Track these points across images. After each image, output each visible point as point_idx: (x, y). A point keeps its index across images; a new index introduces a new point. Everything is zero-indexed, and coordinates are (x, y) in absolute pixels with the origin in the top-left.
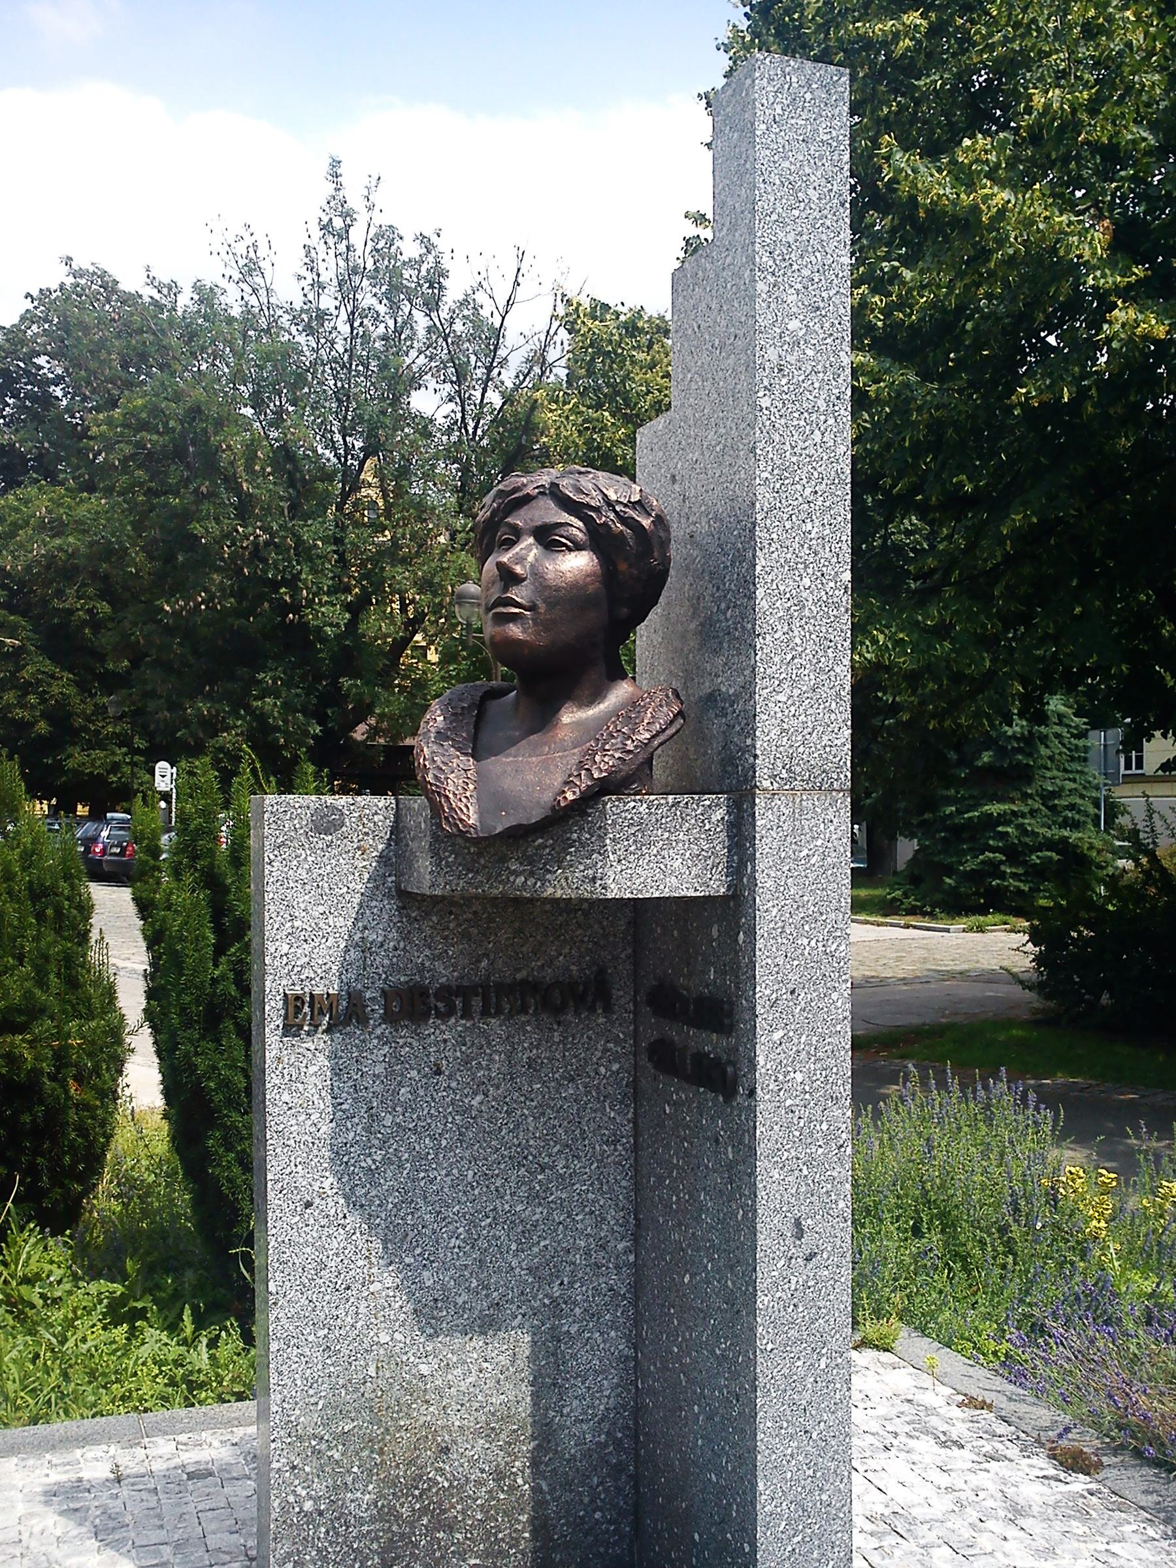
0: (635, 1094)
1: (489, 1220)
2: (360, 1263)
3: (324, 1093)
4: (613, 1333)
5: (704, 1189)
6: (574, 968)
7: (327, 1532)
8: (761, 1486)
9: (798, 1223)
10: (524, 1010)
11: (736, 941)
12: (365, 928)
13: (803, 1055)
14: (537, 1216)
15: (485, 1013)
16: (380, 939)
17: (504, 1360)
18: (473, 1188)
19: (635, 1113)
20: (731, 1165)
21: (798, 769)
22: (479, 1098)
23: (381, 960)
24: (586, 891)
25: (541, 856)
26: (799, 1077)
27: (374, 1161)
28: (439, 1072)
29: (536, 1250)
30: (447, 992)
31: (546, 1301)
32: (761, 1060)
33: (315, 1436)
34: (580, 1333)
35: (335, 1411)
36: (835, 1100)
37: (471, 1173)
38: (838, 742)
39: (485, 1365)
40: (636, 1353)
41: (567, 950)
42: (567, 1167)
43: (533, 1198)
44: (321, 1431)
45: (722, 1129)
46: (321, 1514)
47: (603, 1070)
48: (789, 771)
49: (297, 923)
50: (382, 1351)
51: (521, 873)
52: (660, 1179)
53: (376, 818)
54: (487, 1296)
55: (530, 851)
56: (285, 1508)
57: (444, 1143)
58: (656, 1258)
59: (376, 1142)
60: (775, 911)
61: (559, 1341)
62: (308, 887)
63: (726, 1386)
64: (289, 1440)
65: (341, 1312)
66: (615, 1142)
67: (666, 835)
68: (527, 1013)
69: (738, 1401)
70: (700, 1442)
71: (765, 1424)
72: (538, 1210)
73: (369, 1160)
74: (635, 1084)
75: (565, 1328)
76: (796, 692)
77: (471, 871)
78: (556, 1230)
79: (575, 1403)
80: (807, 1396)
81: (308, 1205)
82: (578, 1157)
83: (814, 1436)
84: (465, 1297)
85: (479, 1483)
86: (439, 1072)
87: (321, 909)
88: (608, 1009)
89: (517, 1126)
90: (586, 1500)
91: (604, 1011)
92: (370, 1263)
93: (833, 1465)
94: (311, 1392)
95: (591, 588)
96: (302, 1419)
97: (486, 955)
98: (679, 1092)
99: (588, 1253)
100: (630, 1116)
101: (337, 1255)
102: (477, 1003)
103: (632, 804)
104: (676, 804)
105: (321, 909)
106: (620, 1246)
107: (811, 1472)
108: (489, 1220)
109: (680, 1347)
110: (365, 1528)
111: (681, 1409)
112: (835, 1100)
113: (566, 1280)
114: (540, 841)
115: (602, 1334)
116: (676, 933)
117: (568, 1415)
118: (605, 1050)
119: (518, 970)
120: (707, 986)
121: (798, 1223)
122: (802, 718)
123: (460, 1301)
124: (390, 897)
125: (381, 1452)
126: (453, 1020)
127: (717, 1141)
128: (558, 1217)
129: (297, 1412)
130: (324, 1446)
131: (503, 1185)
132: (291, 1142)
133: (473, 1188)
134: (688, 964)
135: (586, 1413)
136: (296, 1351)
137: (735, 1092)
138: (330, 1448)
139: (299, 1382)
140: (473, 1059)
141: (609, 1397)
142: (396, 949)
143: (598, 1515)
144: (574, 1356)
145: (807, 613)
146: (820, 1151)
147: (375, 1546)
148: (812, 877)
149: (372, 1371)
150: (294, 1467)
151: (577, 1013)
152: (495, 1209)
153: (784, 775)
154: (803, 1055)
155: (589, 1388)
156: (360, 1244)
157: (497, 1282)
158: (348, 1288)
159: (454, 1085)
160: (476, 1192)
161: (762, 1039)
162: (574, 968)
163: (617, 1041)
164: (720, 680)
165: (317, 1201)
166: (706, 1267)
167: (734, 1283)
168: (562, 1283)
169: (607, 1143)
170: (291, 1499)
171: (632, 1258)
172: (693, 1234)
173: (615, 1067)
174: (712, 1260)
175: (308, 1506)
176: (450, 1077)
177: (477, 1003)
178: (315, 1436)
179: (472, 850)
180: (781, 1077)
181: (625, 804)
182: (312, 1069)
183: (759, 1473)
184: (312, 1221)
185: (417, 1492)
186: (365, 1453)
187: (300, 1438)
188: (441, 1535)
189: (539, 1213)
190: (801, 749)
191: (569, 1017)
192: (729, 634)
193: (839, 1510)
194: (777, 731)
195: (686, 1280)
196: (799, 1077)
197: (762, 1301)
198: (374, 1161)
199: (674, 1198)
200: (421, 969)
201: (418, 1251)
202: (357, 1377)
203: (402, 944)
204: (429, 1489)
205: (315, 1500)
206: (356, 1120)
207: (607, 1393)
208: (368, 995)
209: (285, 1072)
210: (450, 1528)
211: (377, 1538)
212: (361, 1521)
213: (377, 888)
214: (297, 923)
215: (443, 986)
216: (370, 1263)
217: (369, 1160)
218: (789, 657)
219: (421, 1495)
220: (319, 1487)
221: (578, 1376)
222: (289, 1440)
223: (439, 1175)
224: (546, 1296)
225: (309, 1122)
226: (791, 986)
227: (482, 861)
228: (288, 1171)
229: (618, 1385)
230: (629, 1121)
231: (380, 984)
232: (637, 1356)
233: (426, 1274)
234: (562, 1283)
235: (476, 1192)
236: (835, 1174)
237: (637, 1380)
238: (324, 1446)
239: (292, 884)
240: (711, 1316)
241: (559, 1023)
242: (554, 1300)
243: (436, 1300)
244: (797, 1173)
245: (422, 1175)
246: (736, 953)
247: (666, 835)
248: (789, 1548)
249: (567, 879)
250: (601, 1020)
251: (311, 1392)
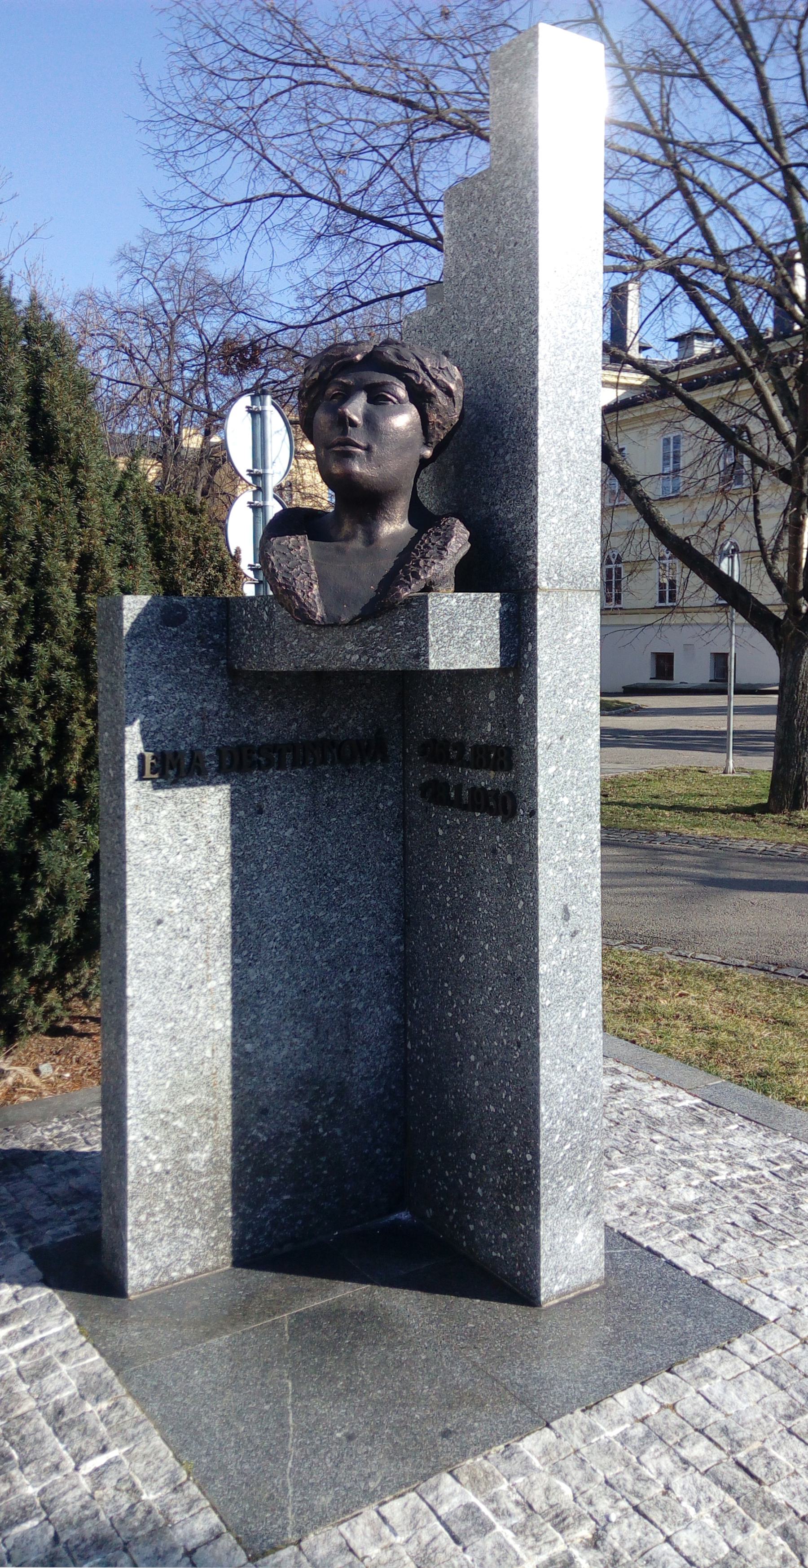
0: (404, 823)
1: (298, 925)
2: (201, 966)
3: (172, 832)
4: (388, 1008)
5: (481, 889)
6: (359, 728)
7: (173, 1187)
8: (543, 1109)
9: (566, 910)
10: (324, 762)
11: (516, 701)
12: (204, 700)
13: (569, 784)
14: (334, 920)
15: (294, 765)
16: (216, 709)
17: (309, 1034)
18: (286, 900)
19: (404, 838)
20: (510, 869)
21: (565, 574)
22: (291, 830)
23: (215, 724)
24: (411, 665)
25: (373, 640)
26: (566, 800)
27: (212, 884)
28: (260, 811)
29: (333, 946)
30: (292, 746)
31: (340, 985)
32: (540, 788)
33: (163, 1111)
34: (365, 1009)
35: (178, 1088)
36: (590, 816)
37: (284, 889)
38: (592, 555)
39: (295, 1040)
40: (406, 1021)
41: (354, 715)
42: (355, 880)
43: (330, 906)
44: (168, 1106)
45: (501, 842)
46: (167, 1173)
47: (381, 806)
48: (559, 575)
49: (151, 698)
50: (217, 1036)
51: (356, 652)
52: (432, 886)
53: (212, 614)
54: (296, 985)
55: (364, 635)
56: (140, 1172)
57: (265, 866)
58: (428, 946)
59: (213, 869)
60: (550, 678)
61: (349, 1016)
62: (159, 669)
63: (505, 1037)
64: (143, 1116)
65: (184, 1007)
66: (389, 860)
67: (470, 622)
68: (326, 764)
69: (519, 1046)
70: (477, 1083)
71: (545, 1062)
72: (334, 915)
73: (208, 884)
74: (403, 815)
75: (354, 1006)
76: (564, 517)
77: (312, 652)
78: (347, 930)
79: (362, 1064)
80: (573, 1038)
81: (159, 922)
82: (364, 873)
83: (579, 1069)
84: (280, 987)
85: (290, 1135)
86: (260, 811)
87: (169, 686)
88: (385, 760)
89: (319, 851)
90: (370, 1140)
91: (382, 760)
92: (209, 966)
93: (590, 1090)
94: (161, 1075)
95: (410, 434)
96: (153, 1098)
97: (296, 720)
98: (452, 817)
99: (371, 946)
100: (400, 840)
101: (182, 960)
102: (289, 756)
103: (446, 599)
104: (476, 599)
105: (169, 686)
106: (394, 939)
107: (576, 1097)
108: (298, 925)
109: (455, 1012)
110: (203, 1180)
111: (456, 1060)
112: (590, 816)
113: (355, 967)
114: (372, 627)
115: (381, 1009)
116: (449, 699)
117: (356, 1074)
118: (383, 791)
119: (319, 731)
120: (484, 737)
121: (566, 910)
122: (568, 536)
123: (276, 990)
124: (222, 675)
125: (215, 1118)
126: (271, 771)
127: (494, 852)
128: (349, 919)
129: (149, 1093)
130: (170, 1118)
131: (309, 897)
132: (147, 873)
133: (286, 900)
134: (462, 722)
135: (369, 1072)
136: (148, 1043)
137: (514, 813)
138: (174, 1119)
139: (151, 1068)
140: (286, 800)
141: (386, 1058)
142: (227, 716)
143: (378, 1151)
144: (361, 1028)
145: (572, 458)
146: (580, 855)
147: (210, 1194)
148: (574, 654)
149: (208, 1053)
150: (146, 1138)
151: (363, 763)
152: (302, 916)
153: (556, 578)
154: (569, 784)
155: (371, 1052)
156: (201, 951)
157: (304, 974)
158: (191, 987)
159: (272, 821)
160: (289, 904)
161: (541, 772)
162: (359, 728)
163: (392, 784)
164: (497, 507)
165: (167, 919)
166: (483, 947)
167: (514, 957)
168: (352, 971)
169: (384, 861)
170: (144, 1164)
171: (402, 948)
172: (469, 924)
173: (390, 803)
174: (489, 941)
175: (158, 1168)
176: (269, 815)
177: (289, 756)
178: (163, 1111)
179: (313, 635)
180: (554, 801)
181: (441, 598)
182: (164, 813)
183: (542, 1100)
184: (162, 936)
185: (243, 1147)
186: (203, 1120)
187: (151, 1114)
188: (261, 1179)
189: (334, 917)
190: (567, 559)
191: (357, 766)
192: (508, 472)
193: (594, 1123)
194: (550, 545)
195: (461, 960)
196: (566, 800)
197: (543, 968)
198: (212, 884)
199: (448, 899)
200: (247, 732)
201: (245, 953)
202: (196, 1060)
203: (232, 713)
204: (252, 1144)
205: (164, 1162)
206: (197, 852)
207: (384, 1055)
208: (207, 753)
209: (142, 816)
210: (268, 1174)
211: (212, 1188)
212: (199, 1174)
213: (213, 669)
214: (151, 698)
215: (263, 745)
216: (209, 966)
217: (208, 884)
218: (559, 490)
219: (246, 1149)
220: (167, 1151)
221: (364, 1042)
222: (143, 1116)
223: (261, 892)
224: (341, 981)
225: (161, 856)
226: (560, 734)
227: (322, 644)
228: (144, 895)
229: (392, 1048)
230: (400, 843)
231: (215, 744)
232: (406, 1024)
233: (251, 971)
234: (352, 971)
235: (289, 904)
236: (590, 871)
237: (406, 1043)
238: (170, 1118)
239: (146, 667)
240: (489, 985)
241: (349, 771)
242: (346, 985)
243: (258, 992)
244: (564, 871)
245: (248, 893)
246: (516, 711)
247: (470, 622)
248: (562, 1154)
249: (395, 655)
250: (380, 768)
251: (161, 1075)
